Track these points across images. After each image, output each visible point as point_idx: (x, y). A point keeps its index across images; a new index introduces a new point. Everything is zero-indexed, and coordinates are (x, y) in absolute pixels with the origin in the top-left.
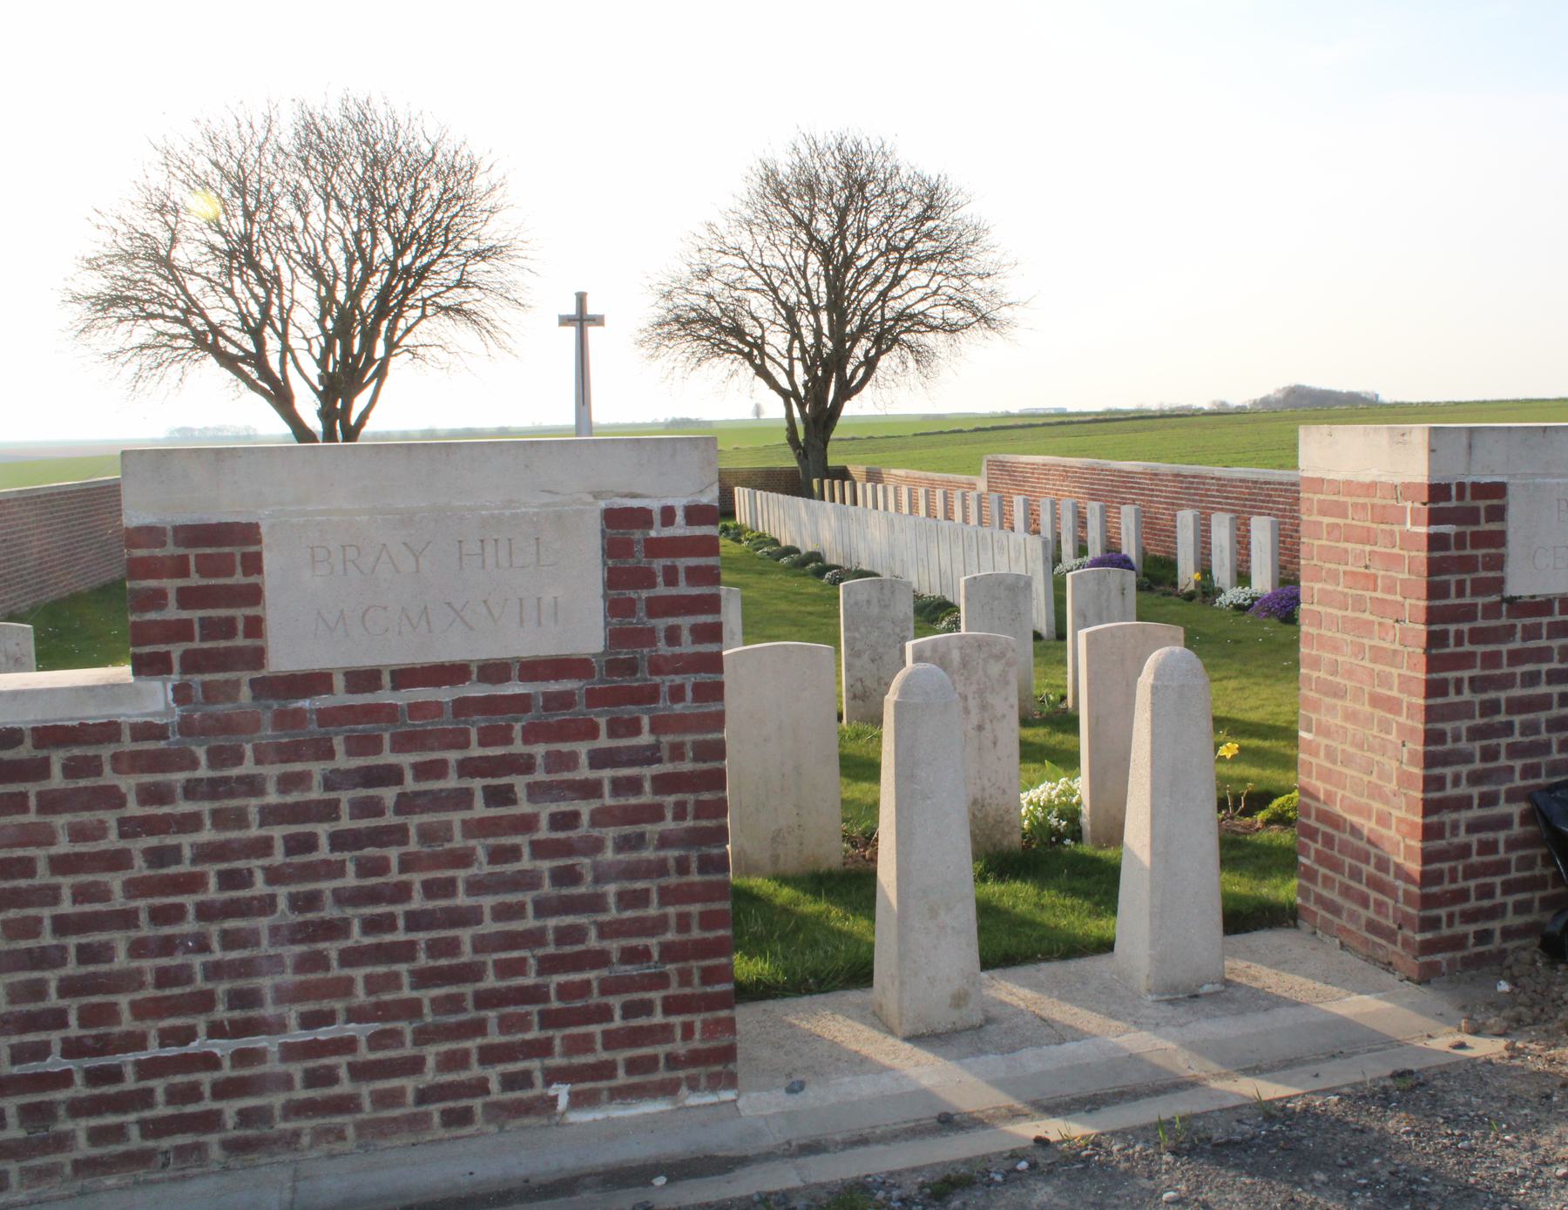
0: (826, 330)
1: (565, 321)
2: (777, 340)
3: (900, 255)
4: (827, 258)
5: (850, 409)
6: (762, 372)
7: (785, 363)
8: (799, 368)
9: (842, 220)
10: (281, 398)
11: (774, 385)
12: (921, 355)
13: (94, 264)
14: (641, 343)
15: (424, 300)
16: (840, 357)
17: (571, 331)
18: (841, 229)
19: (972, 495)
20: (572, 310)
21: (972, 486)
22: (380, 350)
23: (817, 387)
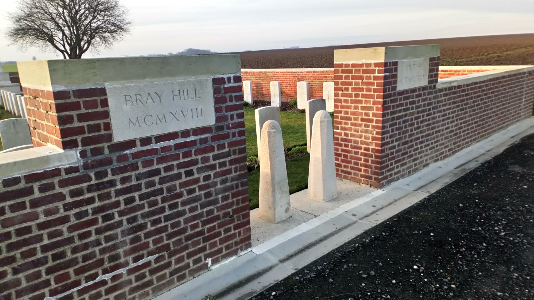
14: (11, 36)
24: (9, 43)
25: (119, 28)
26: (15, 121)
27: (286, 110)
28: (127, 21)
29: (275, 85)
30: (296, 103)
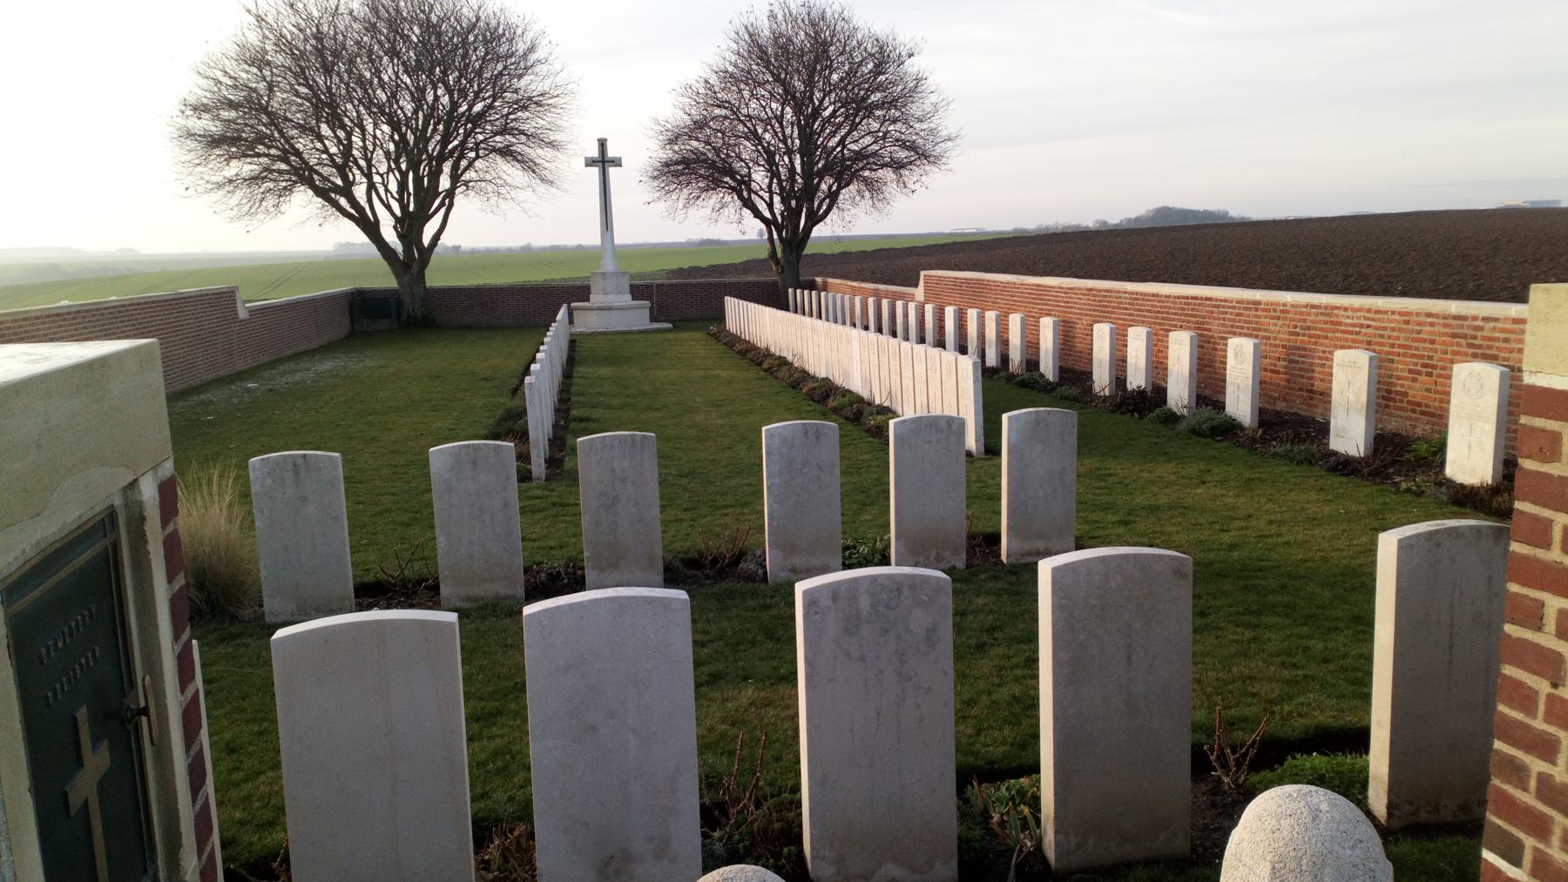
0: (798, 169)
1: (590, 162)
2: (760, 177)
3: (858, 108)
4: (798, 111)
5: (817, 232)
6: (748, 204)
7: (766, 196)
8: (777, 199)
9: (811, 76)
10: (370, 227)
11: (757, 214)
12: (873, 187)
13: (200, 109)
14: (655, 178)
15: (477, 144)
16: (809, 192)
17: (595, 171)
18: (810, 84)
19: (912, 306)
20: (595, 153)
21: (911, 298)
22: (445, 183)
23: (792, 215)
24: (648, 197)
25: (919, 154)
26: (300, 461)
27: (1388, 477)
28: (945, 133)
29: (1353, 365)
30: (1441, 448)
